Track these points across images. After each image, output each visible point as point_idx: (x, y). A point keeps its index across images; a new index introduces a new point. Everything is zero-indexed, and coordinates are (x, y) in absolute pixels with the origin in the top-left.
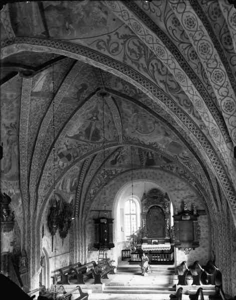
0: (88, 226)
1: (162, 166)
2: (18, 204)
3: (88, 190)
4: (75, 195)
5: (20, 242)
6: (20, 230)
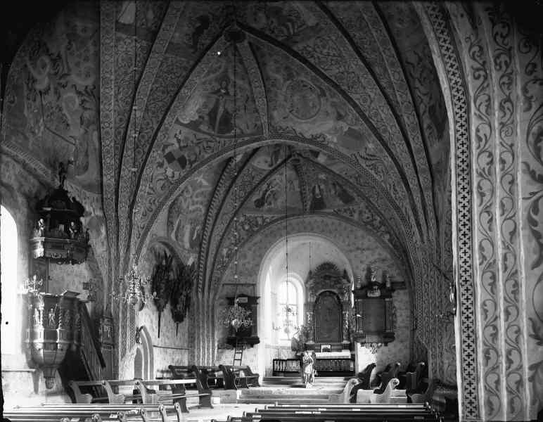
2: (99, 233)
5: (103, 299)
6: (102, 279)
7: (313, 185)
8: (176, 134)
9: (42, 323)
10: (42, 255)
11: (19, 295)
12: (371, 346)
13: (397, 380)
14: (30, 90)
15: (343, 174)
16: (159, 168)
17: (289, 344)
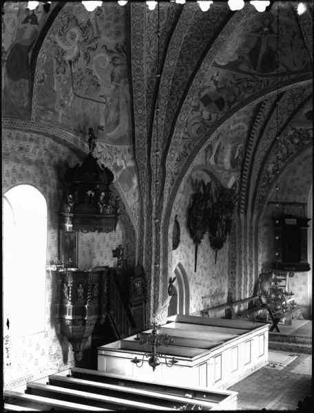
0: (262, 232)
2: (130, 184)
3: (263, 164)
4: (239, 174)
5: (134, 252)
6: (134, 231)
8: (213, 77)
11: (48, 271)
14: (60, 64)
16: (194, 112)
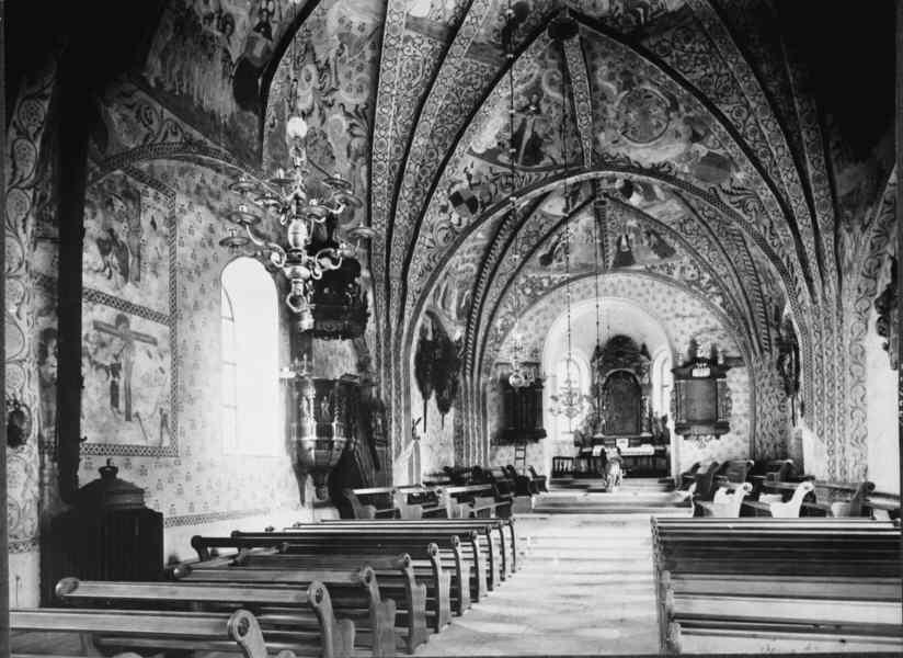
1: (649, 266)
7: (618, 234)
9: (312, 415)
10: (312, 327)
12: (697, 439)
13: (750, 485)
15: (663, 220)
17: (571, 438)
